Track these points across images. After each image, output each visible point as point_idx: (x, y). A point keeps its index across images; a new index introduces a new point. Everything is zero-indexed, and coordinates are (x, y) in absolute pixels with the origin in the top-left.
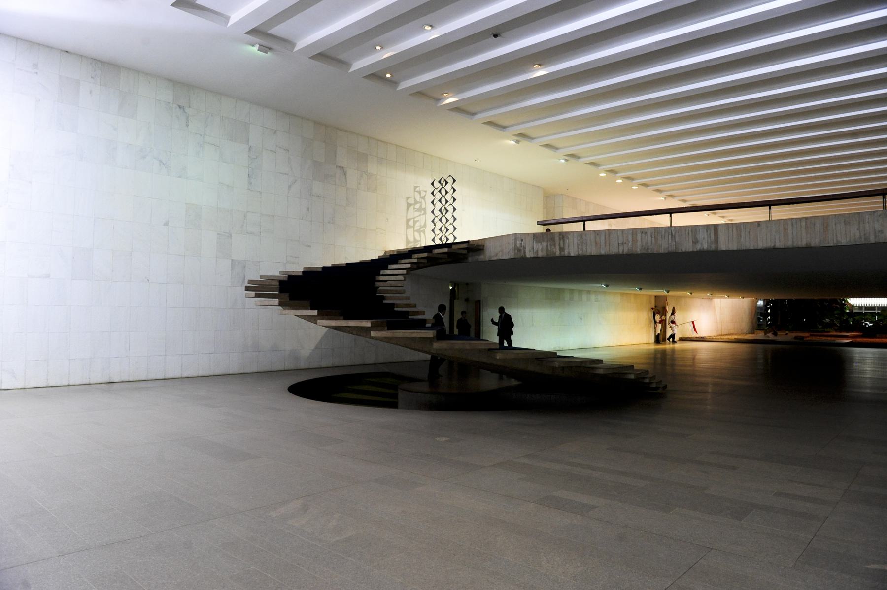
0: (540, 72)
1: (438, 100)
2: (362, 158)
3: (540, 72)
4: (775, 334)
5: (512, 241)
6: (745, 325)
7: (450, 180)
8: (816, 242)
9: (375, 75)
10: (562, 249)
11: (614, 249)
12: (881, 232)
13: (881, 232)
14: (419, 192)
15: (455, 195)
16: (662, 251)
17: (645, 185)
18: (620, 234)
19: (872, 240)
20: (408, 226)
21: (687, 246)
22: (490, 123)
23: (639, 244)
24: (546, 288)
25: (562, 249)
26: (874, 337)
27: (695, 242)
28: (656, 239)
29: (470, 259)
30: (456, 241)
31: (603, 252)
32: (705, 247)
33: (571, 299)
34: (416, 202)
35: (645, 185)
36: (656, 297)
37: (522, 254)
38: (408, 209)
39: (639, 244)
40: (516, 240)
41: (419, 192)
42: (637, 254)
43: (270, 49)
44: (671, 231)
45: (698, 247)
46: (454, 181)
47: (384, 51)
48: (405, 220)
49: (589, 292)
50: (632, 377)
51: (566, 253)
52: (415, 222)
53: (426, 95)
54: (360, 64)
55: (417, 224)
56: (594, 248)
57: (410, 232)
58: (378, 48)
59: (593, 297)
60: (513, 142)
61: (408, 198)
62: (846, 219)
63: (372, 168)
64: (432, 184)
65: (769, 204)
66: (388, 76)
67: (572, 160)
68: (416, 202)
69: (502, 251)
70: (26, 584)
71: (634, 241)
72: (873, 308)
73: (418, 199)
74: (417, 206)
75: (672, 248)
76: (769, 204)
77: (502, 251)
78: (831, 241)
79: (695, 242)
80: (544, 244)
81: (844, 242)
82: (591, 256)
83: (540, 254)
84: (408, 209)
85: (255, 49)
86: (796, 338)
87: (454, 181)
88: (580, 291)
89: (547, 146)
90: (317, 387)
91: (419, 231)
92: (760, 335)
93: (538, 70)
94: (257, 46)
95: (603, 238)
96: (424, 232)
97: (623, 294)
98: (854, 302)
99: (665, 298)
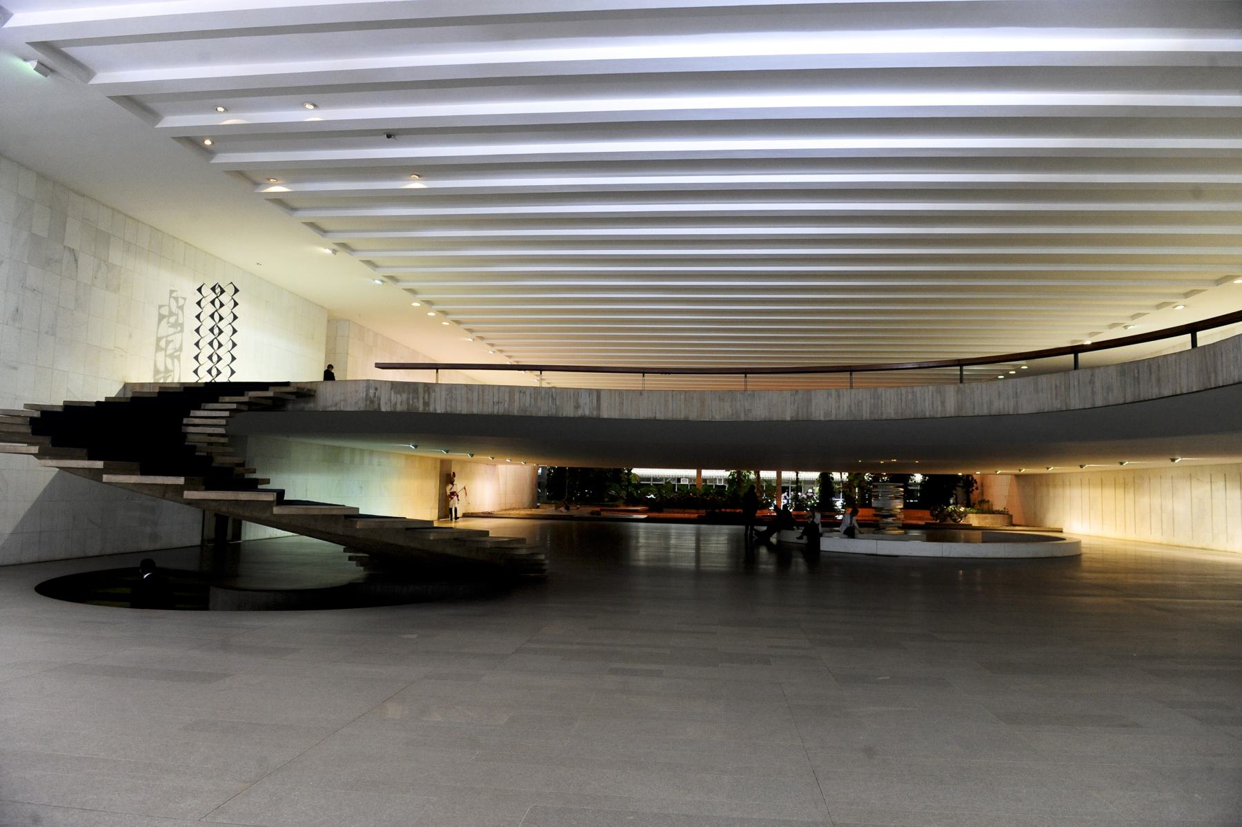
0: (416, 184)
1: (256, 184)
2: (102, 238)
3: (416, 184)
4: (567, 508)
5: (362, 388)
6: (526, 497)
7: (229, 290)
8: (693, 416)
9: (191, 141)
10: (426, 404)
11: (488, 409)
12: (750, 410)
13: (750, 410)
14: (176, 299)
15: (236, 311)
16: (541, 414)
17: (458, 322)
18: (496, 391)
19: (743, 418)
20: (158, 348)
21: (568, 411)
22: (312, 225)
23: (516, 404)
24: (330, 447)
25: (426, 404)
26: (661, 511)
27: (577, 407)
28: (536, 400)
29: (290, 407)
30: (234, 379)
31: (475, 411)
32: (587, 413)
33: (352, 462)
34: (171, 314)
35: (458, 322)
36: (443, 462)
37: (376, 406)
38: (160, 321)
39: (516, 404)
40: (368, 388)
41: (176, 299)
42: (514, 416)
43: (52, 71)
44: (552, 393)
45: (580, 413)
46: (236, 291)
47: (225, 115)
48: (154, 340)
49: (371, 452)
50: (524, 552)
51: (431, 409)
52: (168, 343)
53: (248, 177)
54: (175, 121)
55: (171, 346)
56: (465, 405)
57: (161, 355)
58: (220, 109)
59: (375, 460)
60: (328, 251)
61: (160, 307)
62: (721, 395)
63: (116, 256)
64: (199, 290)
65: (643, 371)
66: (208, 142)
67: (390, 283)
68: (171, 314)
69: (345, 400)
70: (36, 819)
71: (511, 400)
72: (648, 479)
73: (174, 309)
74: (172, 320)
75: (553, 412)
76: (643, 371)
77: (345, 400)
78: (707, 417)
79: (577, 407)
80: (405, 396)
81: (718, 418)
82: (460, 415)
83: (399, 408)
84: (160, 321)
85: (29, 67)
86: (592, 513)
87: (236, 291)
88: (362, 451)
89: (369, 263)
90: (81, 584)
91: (172, 356)
92: (549, 510)
93: (414, 180)
94: (35, 63)
95: (476, 394)
96: (178, 358)
97: (407, 457)
98: (635, 471)
99: (449, 462)
